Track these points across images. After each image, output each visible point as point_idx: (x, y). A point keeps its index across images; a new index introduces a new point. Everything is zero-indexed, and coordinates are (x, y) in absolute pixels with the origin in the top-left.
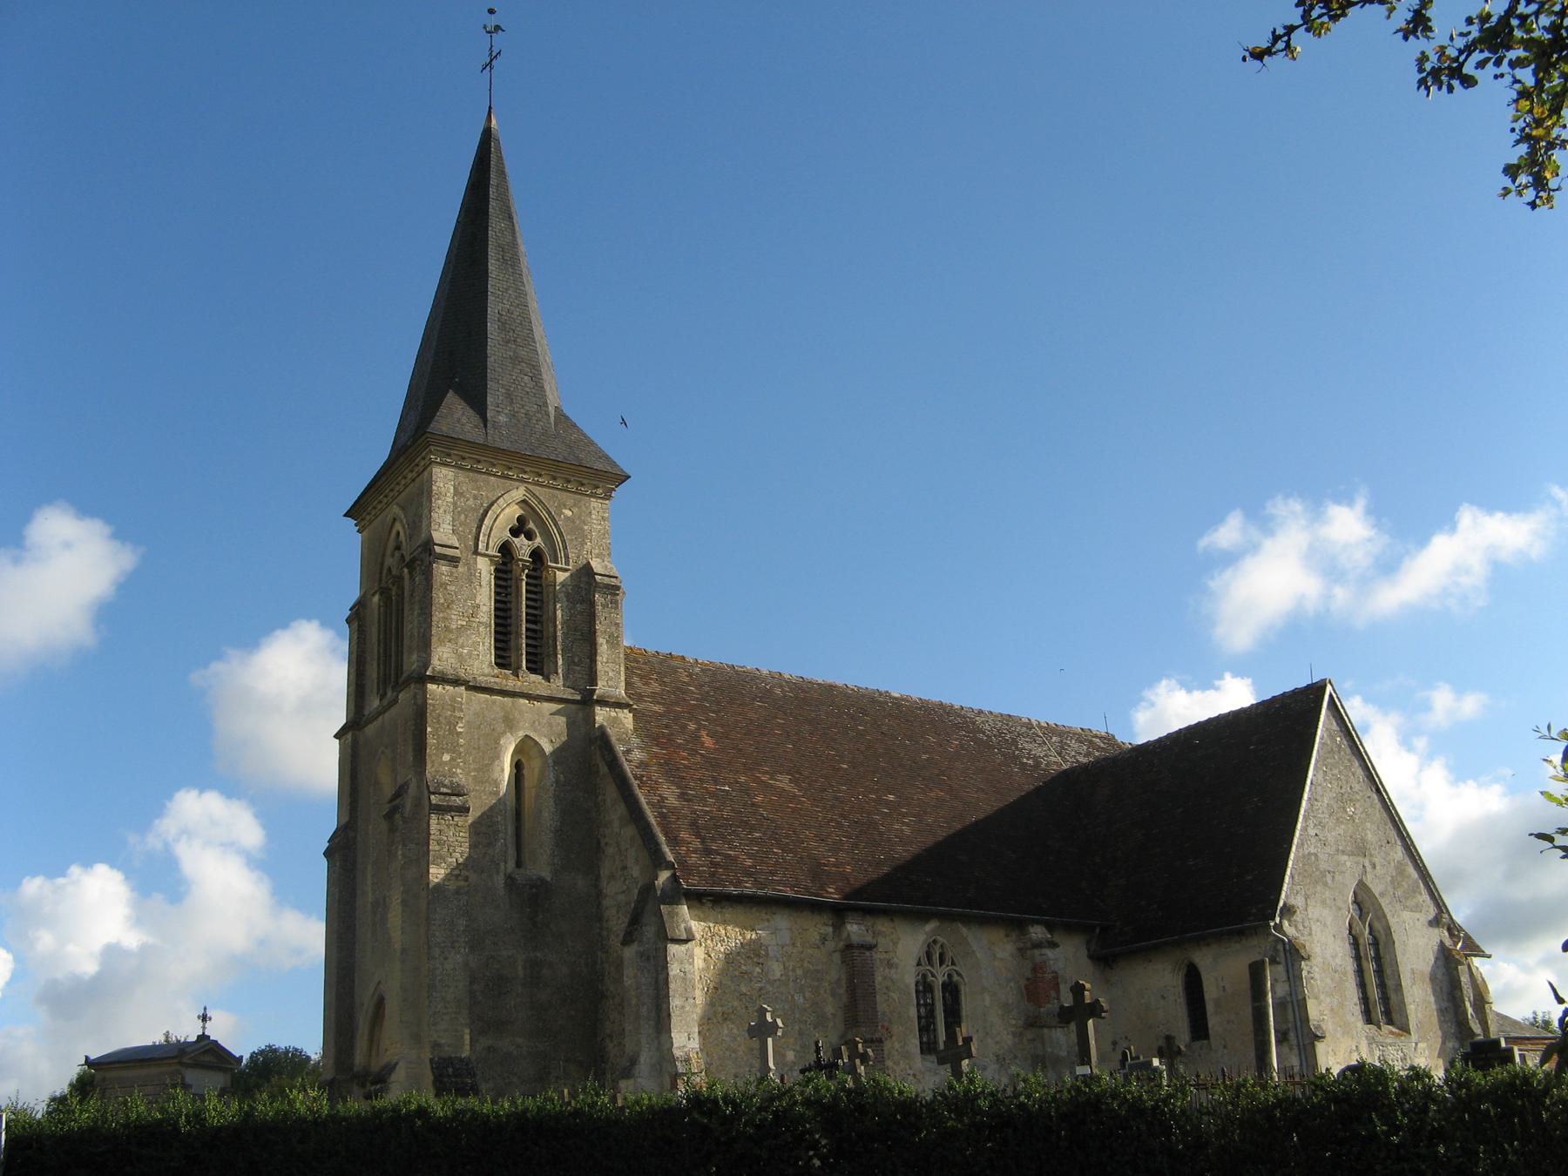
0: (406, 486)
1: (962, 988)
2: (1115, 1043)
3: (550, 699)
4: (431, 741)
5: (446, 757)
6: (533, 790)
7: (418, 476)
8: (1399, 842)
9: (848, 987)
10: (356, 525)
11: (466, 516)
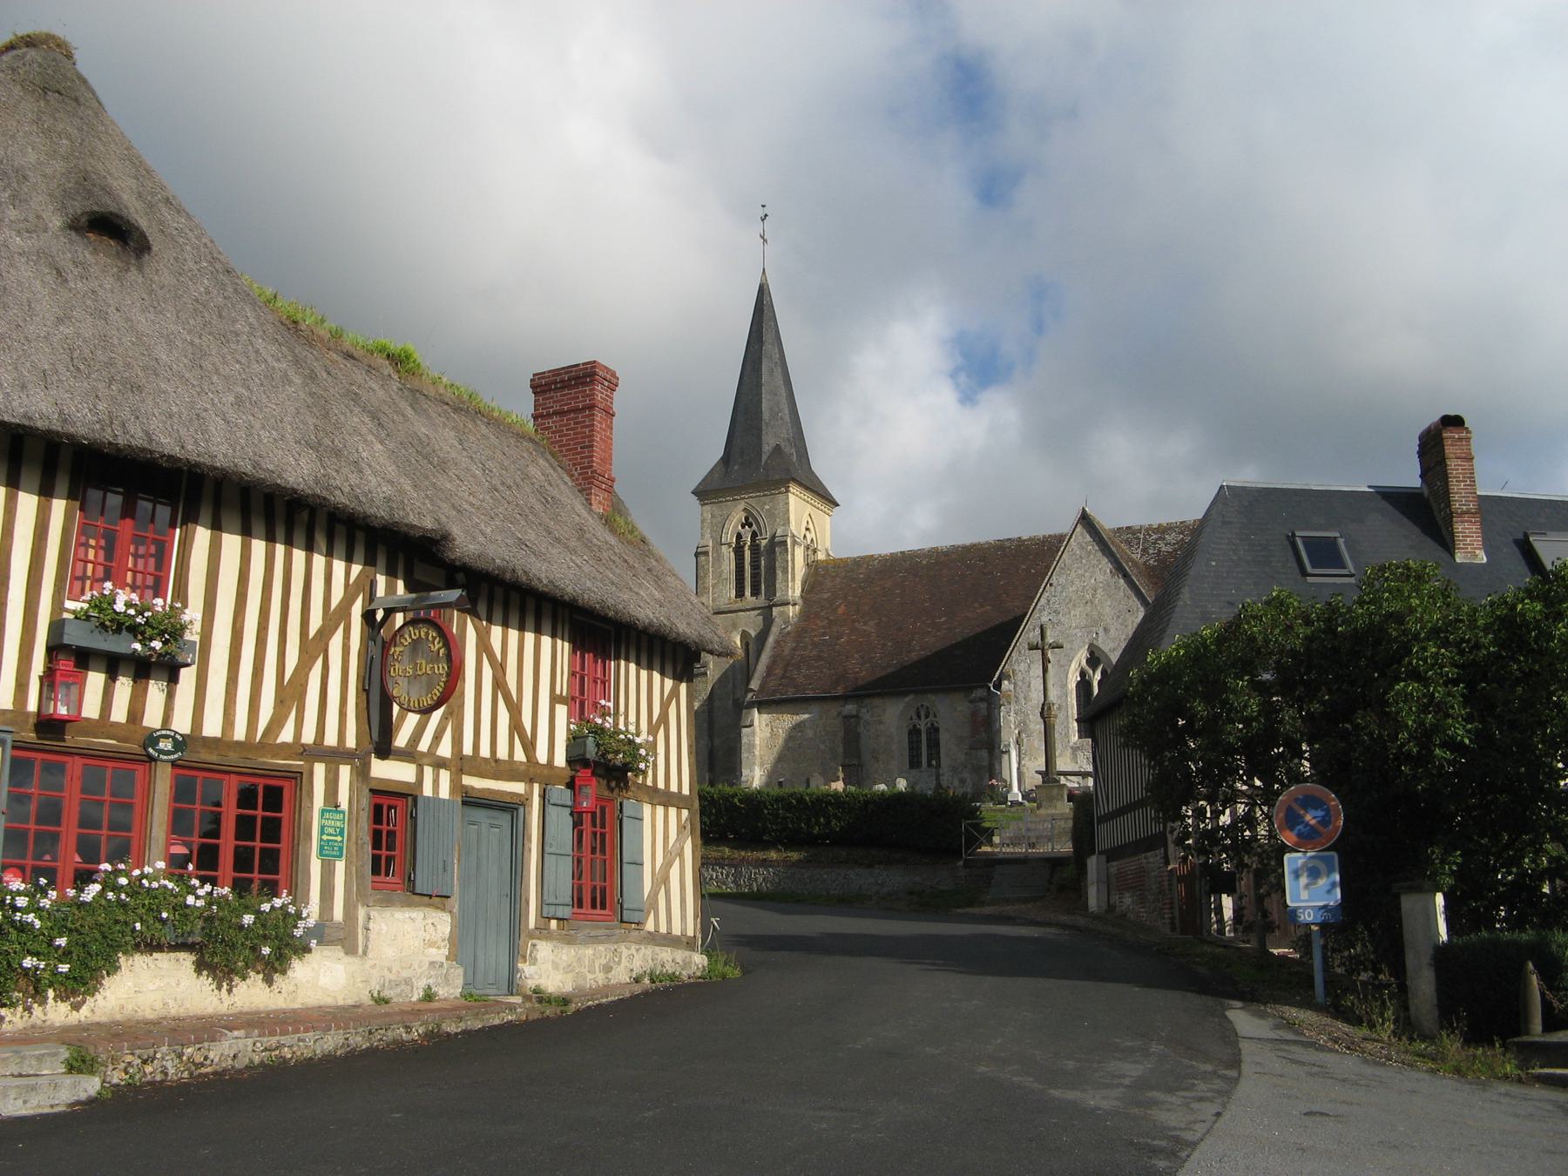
3: (753, 609)
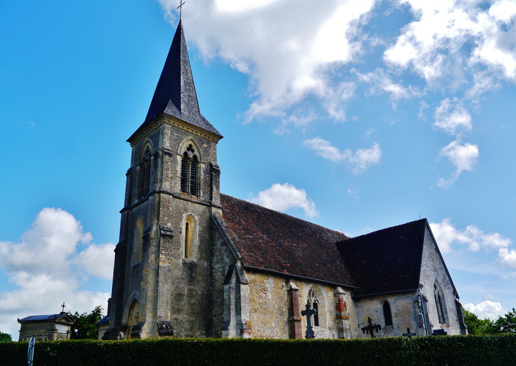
0: (152, 131)
1: (318, 305)
2: (359, 325)
4: (161, 213)
5: (166, 218)
6: (191, 232)
7: (158, 127)
8: (444, 269)
9: (290, 303)
10: (130, 144)
11: (174, 142)
